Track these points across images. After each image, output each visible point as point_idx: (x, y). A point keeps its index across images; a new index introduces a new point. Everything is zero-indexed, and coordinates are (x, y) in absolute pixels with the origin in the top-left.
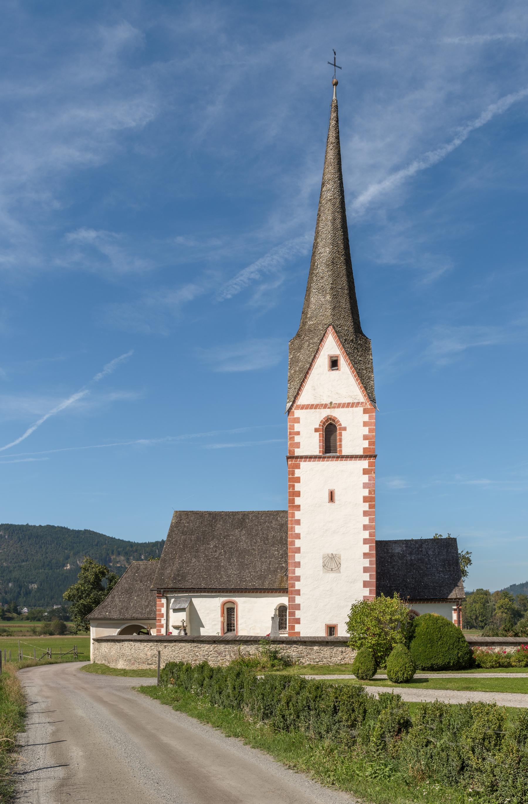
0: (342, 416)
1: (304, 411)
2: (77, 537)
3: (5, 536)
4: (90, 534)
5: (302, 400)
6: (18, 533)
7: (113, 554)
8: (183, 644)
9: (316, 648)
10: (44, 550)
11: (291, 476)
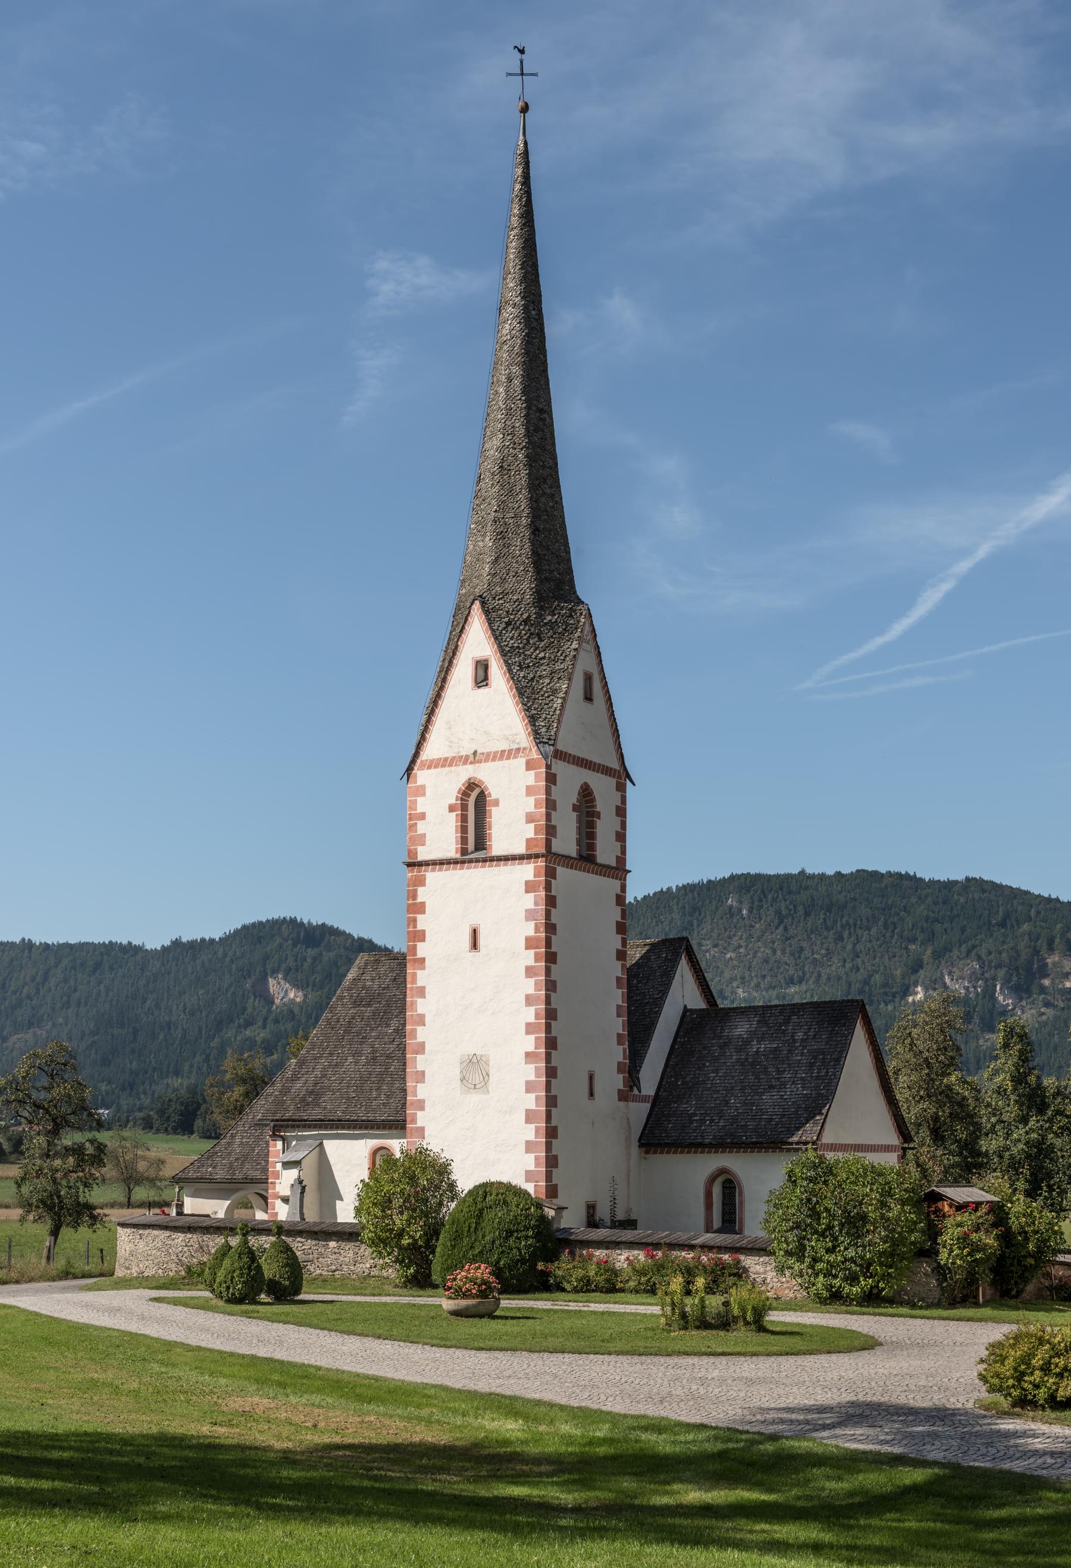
0: (489, 775)
1: (433, 771)
2: (945, 903)
3: (740, 910)
4: (984, 891)
5: (430, 751)
6: (774, 900)
7: (1051, 949)
8: (156, 1232)
9: (332, 1244)
10: (849, 947)
11: (411, 902)
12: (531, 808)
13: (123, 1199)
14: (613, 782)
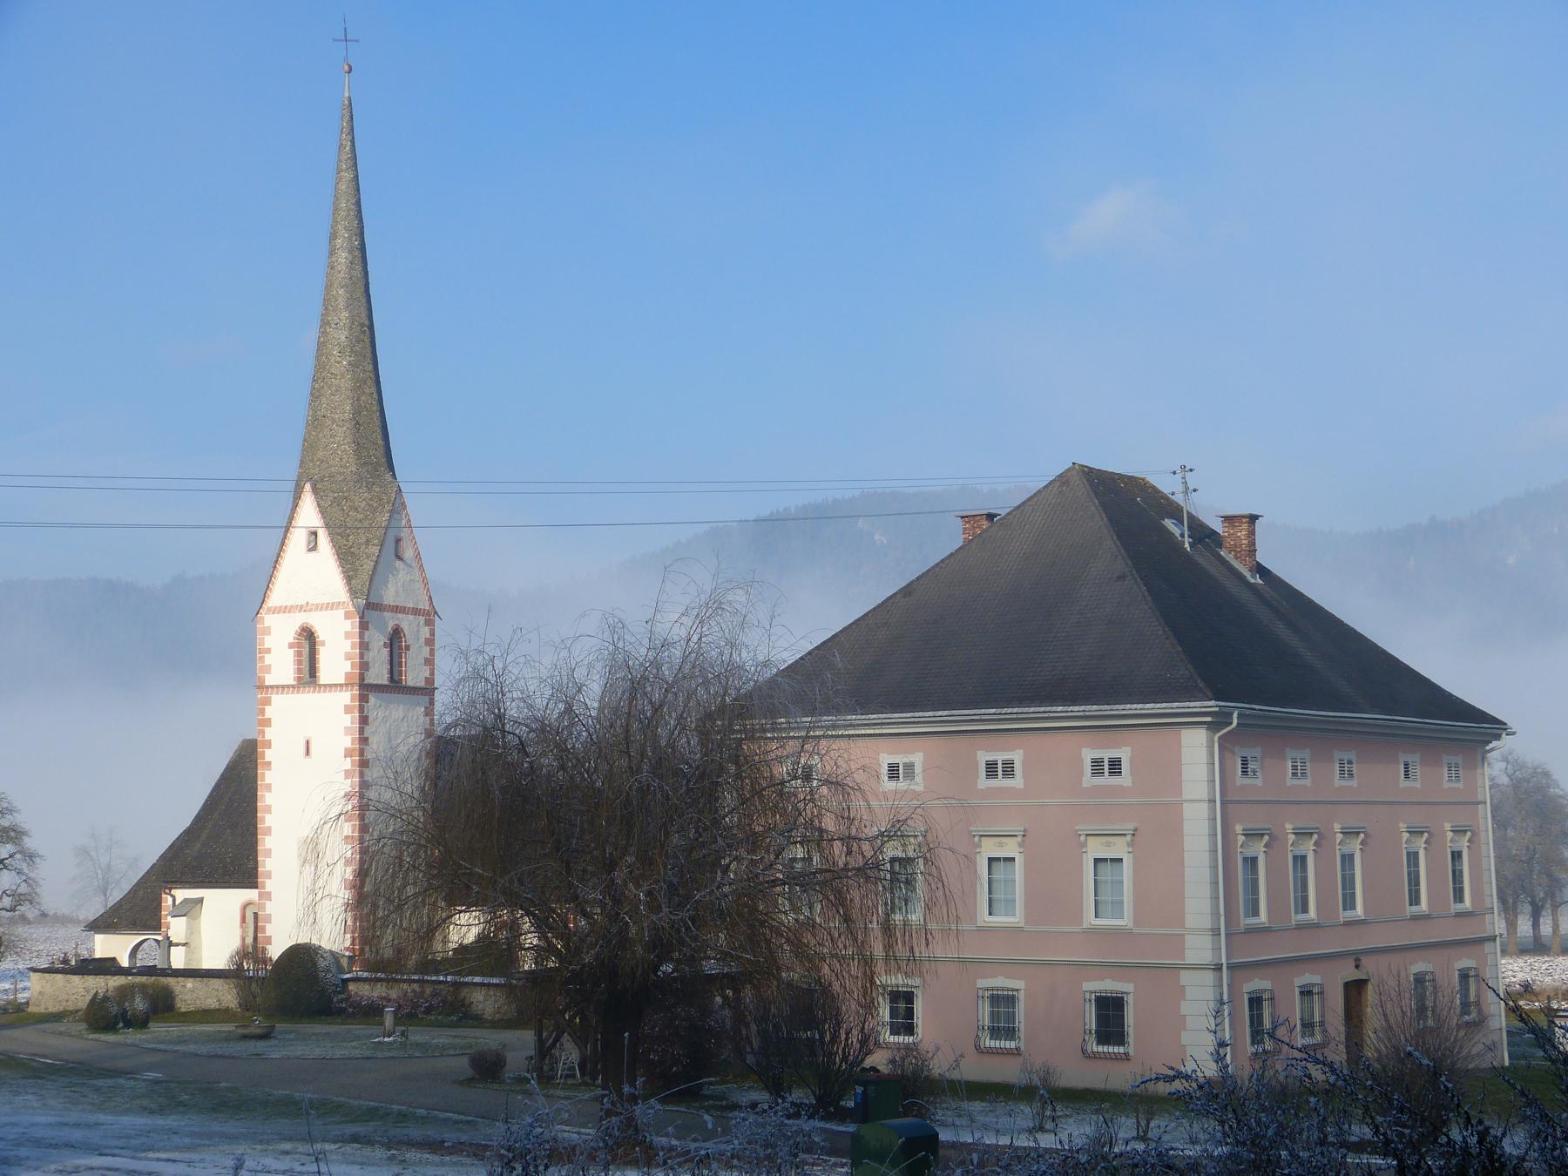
12: (348, 649)
13: (1365, 961)
14: (422, 619)
